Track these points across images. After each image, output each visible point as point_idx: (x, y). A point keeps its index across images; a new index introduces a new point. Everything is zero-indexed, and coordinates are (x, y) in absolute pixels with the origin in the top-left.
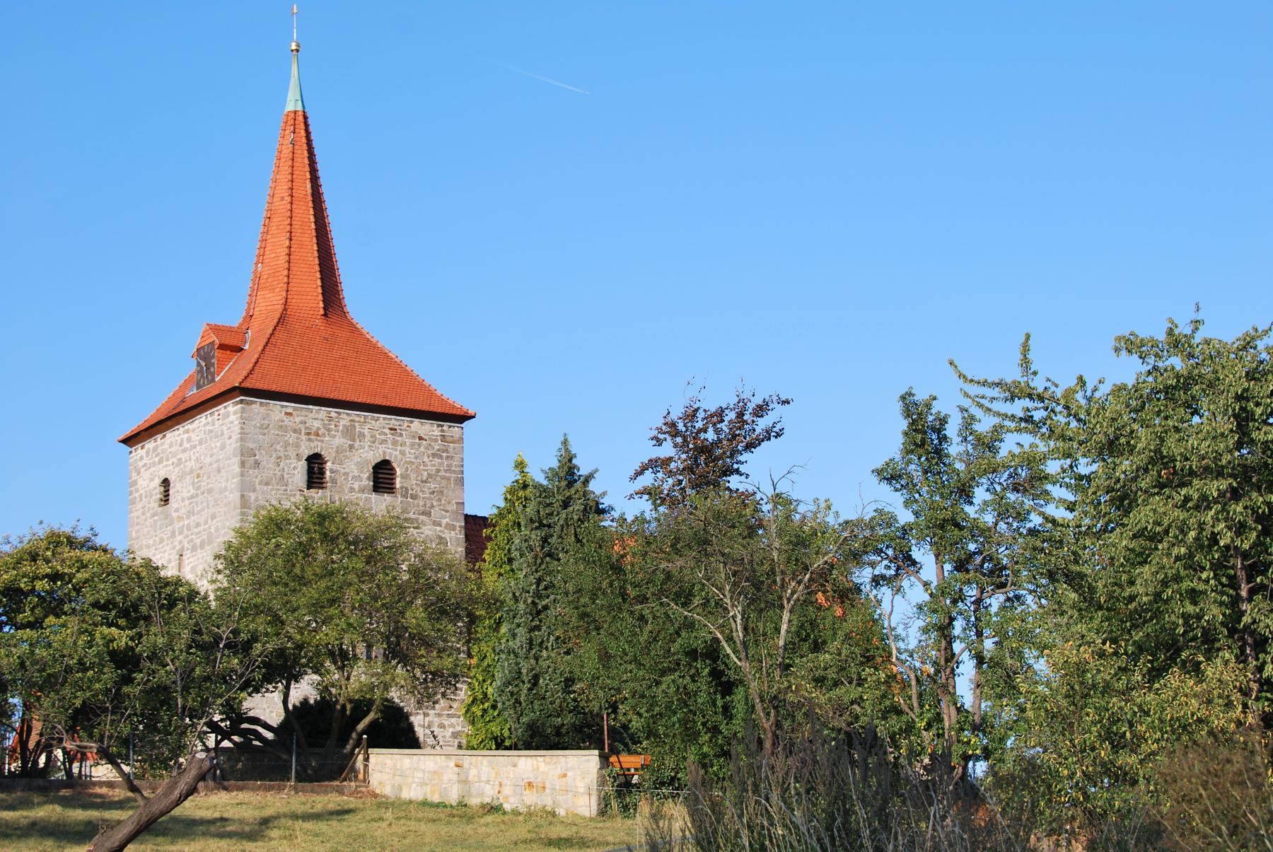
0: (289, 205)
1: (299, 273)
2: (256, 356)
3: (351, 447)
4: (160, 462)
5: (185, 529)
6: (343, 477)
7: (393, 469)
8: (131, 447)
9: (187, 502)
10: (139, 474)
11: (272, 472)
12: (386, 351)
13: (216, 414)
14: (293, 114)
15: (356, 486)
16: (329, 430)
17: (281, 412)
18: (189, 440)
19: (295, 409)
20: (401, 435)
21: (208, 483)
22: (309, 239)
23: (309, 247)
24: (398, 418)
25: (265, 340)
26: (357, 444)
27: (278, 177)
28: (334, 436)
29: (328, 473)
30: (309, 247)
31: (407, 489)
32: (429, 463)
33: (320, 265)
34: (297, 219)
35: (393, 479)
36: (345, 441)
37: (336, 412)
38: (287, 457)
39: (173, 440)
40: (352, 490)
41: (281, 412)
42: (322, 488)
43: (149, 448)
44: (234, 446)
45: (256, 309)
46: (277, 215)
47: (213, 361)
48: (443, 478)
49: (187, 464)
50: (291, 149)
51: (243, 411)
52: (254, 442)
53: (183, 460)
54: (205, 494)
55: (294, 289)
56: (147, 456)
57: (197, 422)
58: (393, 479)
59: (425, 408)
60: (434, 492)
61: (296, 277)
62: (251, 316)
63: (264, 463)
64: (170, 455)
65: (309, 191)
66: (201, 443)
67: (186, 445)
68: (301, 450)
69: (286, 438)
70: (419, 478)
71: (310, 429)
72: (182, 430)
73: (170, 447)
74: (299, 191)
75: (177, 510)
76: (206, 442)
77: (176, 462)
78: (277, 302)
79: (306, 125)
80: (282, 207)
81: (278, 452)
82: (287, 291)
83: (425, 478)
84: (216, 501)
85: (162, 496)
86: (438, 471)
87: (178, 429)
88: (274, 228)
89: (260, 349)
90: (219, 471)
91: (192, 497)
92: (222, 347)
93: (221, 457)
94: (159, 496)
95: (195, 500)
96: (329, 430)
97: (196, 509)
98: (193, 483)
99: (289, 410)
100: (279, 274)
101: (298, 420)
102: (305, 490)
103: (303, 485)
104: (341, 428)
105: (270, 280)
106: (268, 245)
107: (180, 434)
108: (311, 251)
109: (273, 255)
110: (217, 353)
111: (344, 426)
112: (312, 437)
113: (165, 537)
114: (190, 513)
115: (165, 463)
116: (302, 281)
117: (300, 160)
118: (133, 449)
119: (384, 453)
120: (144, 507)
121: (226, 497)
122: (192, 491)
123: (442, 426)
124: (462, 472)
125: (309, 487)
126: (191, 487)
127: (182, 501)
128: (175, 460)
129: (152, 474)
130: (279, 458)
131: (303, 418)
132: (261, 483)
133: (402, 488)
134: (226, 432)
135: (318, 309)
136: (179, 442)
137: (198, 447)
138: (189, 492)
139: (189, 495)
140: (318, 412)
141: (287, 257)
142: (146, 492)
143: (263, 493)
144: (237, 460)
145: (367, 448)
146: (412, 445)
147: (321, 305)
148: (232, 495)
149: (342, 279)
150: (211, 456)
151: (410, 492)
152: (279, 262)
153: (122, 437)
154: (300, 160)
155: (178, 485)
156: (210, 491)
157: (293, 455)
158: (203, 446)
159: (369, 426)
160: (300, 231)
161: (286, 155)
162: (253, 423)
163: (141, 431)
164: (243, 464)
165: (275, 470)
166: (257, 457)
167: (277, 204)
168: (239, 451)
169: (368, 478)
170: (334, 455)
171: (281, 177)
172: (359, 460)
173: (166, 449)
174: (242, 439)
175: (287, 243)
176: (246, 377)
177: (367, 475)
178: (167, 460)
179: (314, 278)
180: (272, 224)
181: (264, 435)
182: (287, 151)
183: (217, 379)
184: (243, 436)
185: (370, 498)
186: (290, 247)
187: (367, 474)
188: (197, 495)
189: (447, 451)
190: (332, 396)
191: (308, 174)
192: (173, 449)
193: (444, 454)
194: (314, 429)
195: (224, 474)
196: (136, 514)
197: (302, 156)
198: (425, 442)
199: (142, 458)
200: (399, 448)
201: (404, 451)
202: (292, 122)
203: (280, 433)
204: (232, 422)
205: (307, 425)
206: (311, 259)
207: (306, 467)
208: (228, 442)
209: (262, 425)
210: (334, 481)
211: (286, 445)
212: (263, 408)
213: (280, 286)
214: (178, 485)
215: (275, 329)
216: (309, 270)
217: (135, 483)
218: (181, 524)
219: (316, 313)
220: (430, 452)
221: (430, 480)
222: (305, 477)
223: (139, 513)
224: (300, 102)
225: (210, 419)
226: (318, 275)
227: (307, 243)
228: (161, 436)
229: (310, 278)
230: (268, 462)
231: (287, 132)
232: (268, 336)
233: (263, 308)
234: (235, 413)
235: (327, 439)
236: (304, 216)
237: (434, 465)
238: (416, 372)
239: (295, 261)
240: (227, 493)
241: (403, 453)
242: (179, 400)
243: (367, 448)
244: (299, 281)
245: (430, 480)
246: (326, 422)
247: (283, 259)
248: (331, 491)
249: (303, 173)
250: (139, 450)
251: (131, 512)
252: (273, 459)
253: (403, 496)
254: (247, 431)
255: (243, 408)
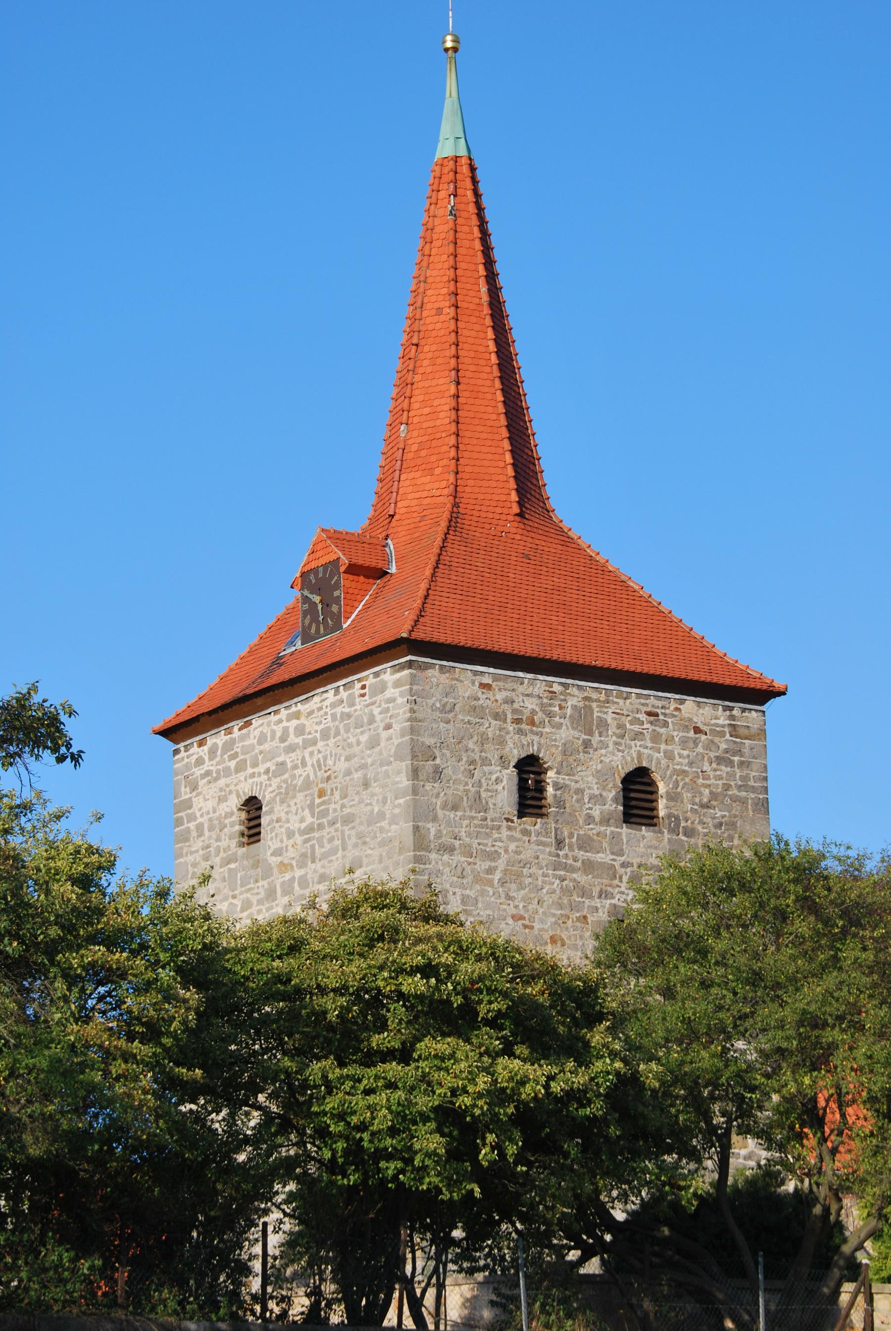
0: (453, 322)
1: (475, 442)
2: (424, 586)
3: (587, 744)
4: (240, 768)
5: (296, 884)
6: (575, 797)
7: (652, 783)
8: (176, 742)
9: (299, 839)
10: (194, 788)
11: (461, 788)
12: (623, 578)
13: (358, 685)
14: (452, 163)
15: (596, 813)
16: (550, 715)
17: (473, 683)
18: (300, 730)
19: (496, 678)
20: (665, 724)
21: (343, 806)
22: (488, 383)
23: (489, 396)
24: (660, 694)
25: (434, 559)
26: (595, 739)
27: (428, 273)
28: (559, 726)
29: (550, 790)
30: (489, 396)
31: (677, 818)
32: (712, 774)
33: (508, 427)
34: (466, 346)
35: (652, 801)
36: (576, 734)
37: (561, 684)
38: (486, 762)
39: (265, 729)
40: (590, 819)
41: (473, 683)
42: (542, 816)
43: (215, 745)
44: (396, 742)
45: (399, 505)
46: (430, 341)
47: (336, 594)
48: (734, 799)
49: (297, 772)
50: (451, 225)
51: (413, 680)
52: (433, 735)
53: (289, 765)
54: (339, 825)
55: (467, 469)
56: (210, 759)
57: (316, 699)
58: (652, 801)
59: (704, 677)
60: (721, 824)
61: (469, 448)
62: (392, 516)
63: (449, 771)
64: (260, 757)
65: (485, 298)
66: (325, 735)
67: (293, 739)
68: (508, 749)
69: (482, 729)
70: (697, 800)
71: (521, 713)
72: (284, 713)
73: (260, 743)
74: (468, 299)
75: (277, 853)
76: (337, 733)
77: (273, 768)
78: (438, 493)
79: (475, 181)
80: (438, 326)
81: (470, 753)
82: (457, 473)
83: (705, 800)
84: (360, 836)
85: (243, 828)
86: (727, 787)
87: (276, 712)
88: (426, 363)
89: (428, 572)
90: (366, 785)
91: (310, 829)
92: (354, 569)
93: (369, 761)
94: (238, 828)
95: (316, 834)
96: (550, 715)
97: (318, 851)
98: (311, 807)
99: (487, 680)
100: (440, 442)
101: (500, 696)
102: (515, 819)
103: (511, 809)
104: (569, 711)
105: (423, 453)
106: (416, 392)
107: (281, 721)
108: (493, 403)
109: (427, 410)
110: (345, 580)
111: (574, 707)
112: (524, 726)
113: (254, 900)
114: (304, 859)
115: (250, 770)
116: (481, 456)
117: (466, 243)
118: (181, 746)
119: (640, 755)
120: (208, 847)
121: (382, 830)
122: (309, 820)
123: (731, 709)
124: (766, 790)
125: (521, 815)
126: (307, 812)
127: (289, 837)
128: (271, 765)
129: (221, 790)
130: (472, 762)
131: (508, 694)
132: (444, 807)
133: (669, 816)
134: (378, 718)
135: (508, 505)
136: (278, 734)
137: (320, 744)
138: (302, 820)
139: (303, 825)
140: (532, 682)
141: (453, 412)
142: (210, 820)
143: (449, 824)
144: (405, 765)
145: (611, 746)
146: (684, 742)
147: (514, 497)
148: (394, 827)
149: (541, 451)
150: (348, 759)
151: (683, 824)
152: (438, 423)
153: (159, 724)
154: (466, 243)
155: (280, 811)
156: (348, 820)
157: (494, 757)
158: (332, 741)
159: (613, 708)
160: (472, 368)
161: (443, 236)
162: (430, 702)
163: (203, 714)
164: (415, 773)
165: (466, 784)
166: (438, 761)
167: (429, 320)
168: (407, 751)
169: (615, 800)
170: (559, 759)
171: (435, 273)
172: (599, 767)
173: (252, 747)
174: (412, 730)
175: (453, 389)
176: (416, 622)
177: (614, 793)
178: (255, 764)
179: (500, 451)
180: (422, 356)
181: (448, 722)
182: (443, 228)
183: (345, 626)
184: (415, 724)
185: (620, 834)
186: (457, 396)
187: (612, 792)
188: (321, 827)
189: (739, 753)
190: (556, 654)
191: (481, 268)
192: (266, 746)
193: (736, 759)
194: (527, 713)
195: (377, 790)
196: (190, 858)
197: (470, 237)
198: (703, 737)
199: (200, 762)
200: (663, 747)
201: (672, 751)
202: (451, 175)
203: (474, 720)
204: (392, 700)
205: (516, 706)
206: (494, 417)
207: (516, 780)
208: (384, 734)
209: (444, 705)
210: (560, 803)
211: (483, 740)
212: (444, 676)
213: (441, 463)
214: (277, 808)
215: (445, 540)
216: (490, 436)
217: (188, 804)
218: (287, 876)
219: (506, 511)
220: (712, 755)
221: (713, 802)
222: (515, 797)
223: (198, 857)
224: (463, 140)
225: (344, 694)
226: (506, 445)
227: (486, 390)
228: (241, 722)
229: (493, 450)
230: (454, 769)
231: (442, 194)
232: (436, 550)
233: (415, 502)
234: (397, 684)
235: (547, 730)
236: (478, 341)
237: (721, 778)
238: (677, 614)
239: (468, 421)
240: (384, 824)
241: (669, 756)
242: (268, 661)
243: (611, 746)
244: (475, 455)
245: (713, 802)
246: (545, 701)
247: (445, 417)
248: (557, 822)
249: (473, 267)
250: (195, 749)
251: (181, 856)
252: (463, 765)
253: (672, 831)
254: (420, 716)
255: (413, 676)
